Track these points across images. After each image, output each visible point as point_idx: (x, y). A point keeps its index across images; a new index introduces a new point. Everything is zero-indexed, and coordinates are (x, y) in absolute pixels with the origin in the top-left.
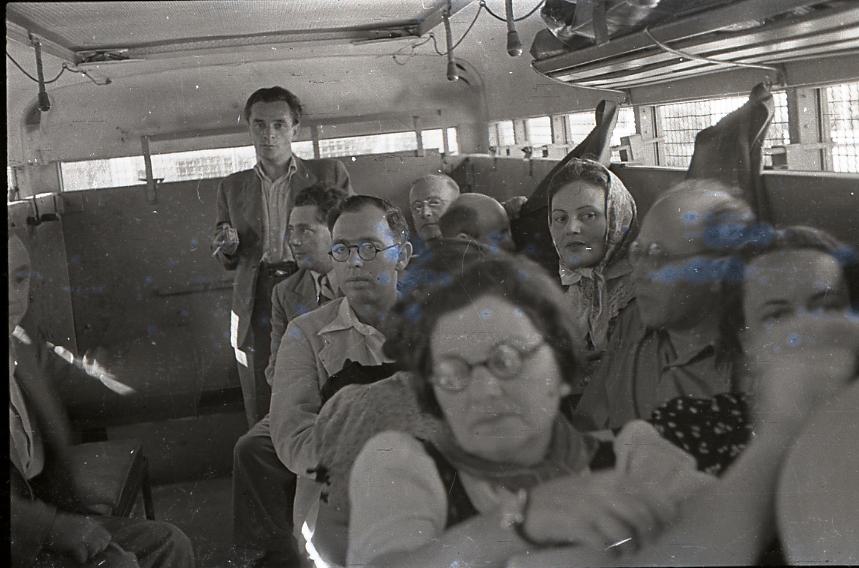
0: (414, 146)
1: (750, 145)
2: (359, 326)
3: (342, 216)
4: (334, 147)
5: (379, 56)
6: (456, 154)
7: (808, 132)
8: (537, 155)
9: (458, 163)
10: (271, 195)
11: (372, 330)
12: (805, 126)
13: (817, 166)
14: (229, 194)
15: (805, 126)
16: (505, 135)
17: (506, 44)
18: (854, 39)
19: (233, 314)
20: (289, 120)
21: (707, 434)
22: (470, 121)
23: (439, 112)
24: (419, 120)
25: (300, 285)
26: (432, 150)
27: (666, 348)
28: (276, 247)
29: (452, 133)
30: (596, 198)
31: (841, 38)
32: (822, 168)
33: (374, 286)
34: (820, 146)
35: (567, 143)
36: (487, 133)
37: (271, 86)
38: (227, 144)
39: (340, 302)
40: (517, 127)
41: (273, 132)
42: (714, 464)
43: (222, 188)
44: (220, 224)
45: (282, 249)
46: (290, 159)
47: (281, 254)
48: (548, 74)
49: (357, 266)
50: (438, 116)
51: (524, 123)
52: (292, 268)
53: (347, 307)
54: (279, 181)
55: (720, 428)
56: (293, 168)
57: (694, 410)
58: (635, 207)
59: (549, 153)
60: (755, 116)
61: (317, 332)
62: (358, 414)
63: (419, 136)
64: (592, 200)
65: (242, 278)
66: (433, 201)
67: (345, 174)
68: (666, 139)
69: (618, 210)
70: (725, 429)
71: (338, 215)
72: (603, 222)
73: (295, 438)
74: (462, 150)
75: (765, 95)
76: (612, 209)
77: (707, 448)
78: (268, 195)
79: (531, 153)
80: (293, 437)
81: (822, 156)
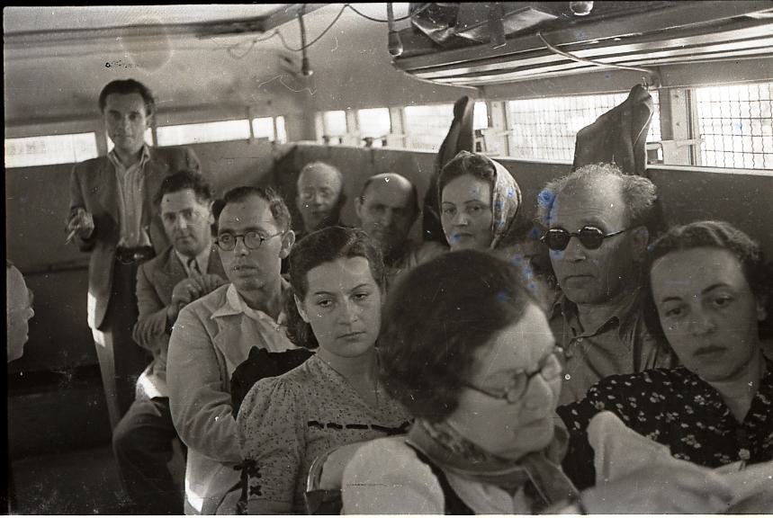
0: (247, 135)
2: (249, 311)
3: (226, 207)
4: (173, 135)
5: (215, 49)
7: (680, 130)
10: (126, 181)
11: (262, 315)
14: (83, 180)
15: (678, 124)
16: (334, 126)
17: (387, 43)
20: (142, 111)
21: (643, 403)
22: (298, 111)
24: (251, 110)
27: (574, 323)
28: (134, 233)
29: (281, 121)
31: (126, 29)
33: (260, 274)
34: (691, 142)
37: (126, 78)
38: (56, 132)
39: (226, 289)
41: (128, 123)
43: (76, 174)
44: (73, 208)
45: (139, 233)
46: (143, 148)
47: (138, 239)
48: (408, 72)
49: (243, 255)
50: (269, 109)
52: (149, 253)
53: (236, 295)
54: (133, 168)
55: (654, 397)
56: (146, 156)
57: (628, 384)
58: (520, 196)
59: (388, 142)
60: (633, 113)
61: (209, 317)
65: (99, 261)
67: (195, 162)
69: (504, 202)
71: (223, 206)
72: (489, 215)
73: (191, 420)
74: (290, 138)
75: (645, 96)
76: (497, 200)
77: (644, 416)
78: (122, 183)
80: (193, 422)
81: (691, 150)
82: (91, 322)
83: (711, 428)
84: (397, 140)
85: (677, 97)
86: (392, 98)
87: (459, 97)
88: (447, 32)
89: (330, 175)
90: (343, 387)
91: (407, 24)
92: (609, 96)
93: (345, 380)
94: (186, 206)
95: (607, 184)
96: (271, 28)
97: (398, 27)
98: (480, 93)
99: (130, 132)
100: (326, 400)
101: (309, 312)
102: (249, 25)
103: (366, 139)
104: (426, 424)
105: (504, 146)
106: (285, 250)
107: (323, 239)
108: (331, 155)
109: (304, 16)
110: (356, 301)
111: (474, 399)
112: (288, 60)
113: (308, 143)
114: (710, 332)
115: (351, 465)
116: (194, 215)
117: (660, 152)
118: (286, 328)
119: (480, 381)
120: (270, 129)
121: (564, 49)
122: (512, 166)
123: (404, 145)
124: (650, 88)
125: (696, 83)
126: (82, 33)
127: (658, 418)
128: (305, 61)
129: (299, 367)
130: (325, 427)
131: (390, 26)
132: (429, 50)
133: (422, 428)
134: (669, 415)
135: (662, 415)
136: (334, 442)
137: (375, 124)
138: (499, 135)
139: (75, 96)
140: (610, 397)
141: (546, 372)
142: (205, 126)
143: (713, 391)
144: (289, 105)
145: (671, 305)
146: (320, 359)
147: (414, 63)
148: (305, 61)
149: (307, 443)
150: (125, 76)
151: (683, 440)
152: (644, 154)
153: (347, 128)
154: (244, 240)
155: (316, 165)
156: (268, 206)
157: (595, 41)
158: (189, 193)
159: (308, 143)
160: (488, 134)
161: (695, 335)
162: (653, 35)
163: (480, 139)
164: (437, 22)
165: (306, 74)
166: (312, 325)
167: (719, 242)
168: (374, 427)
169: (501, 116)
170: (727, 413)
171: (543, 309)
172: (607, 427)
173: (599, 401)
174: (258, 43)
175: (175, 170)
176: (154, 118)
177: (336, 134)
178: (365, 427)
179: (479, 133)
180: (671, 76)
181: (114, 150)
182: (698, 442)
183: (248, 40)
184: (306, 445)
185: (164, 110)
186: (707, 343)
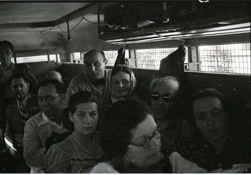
2: (50, 122)
4: (21, 60)
6: (60, 62)
7: (194, 59)
8: (77, 63)
13: (197, 70)
15: (194, 57)
18: (249, 31)
20: (10, 51)
24: (48, 52)
29: (58, 55)
30: (127, 76)
32: (198, 70)
34: (198, 63)
48: (103, 40)
50: (54, 51)
54: (9, 71)
56: (13, 67)
59: (80, 62)
60: (180, 54)
62: (60, 153)
64: (127, 77)
74: (62, 61)
75: (184, 48)
76: (132, 80)
85: (193, 49)
90: (81, 146)
91: (104, 24)
92: (170, 48)
94: (21, 83)
96: (57, 25)
97: (101, 25)
98: (127, 47)
99: (6, 58)
101: (75, 118)
105: (134, 64)
110: (91, 117)
113: (68, 63)
116: (23, 87)
117: (188, 67)
118: (7, 136)
119: (133, 140)
121: (157, 33)
122: (134, 70)
124: (185, 46)
128: (69, 36)
129: (66, 139)
131: (99, 25)
138: (133, 61)
141: (156, 136)
146: (73, 136)
148: (69, 36)
152: (184, 67)
153: (81, 58)
157: (167, 31)
159: (68, 63)
160: (129, 60)
162: (185, 30)
168: (92, 160)
169: (196, 53)
172: (175, 155)
177: (77, 60)
179: (126, 59)
180: (190, 42)
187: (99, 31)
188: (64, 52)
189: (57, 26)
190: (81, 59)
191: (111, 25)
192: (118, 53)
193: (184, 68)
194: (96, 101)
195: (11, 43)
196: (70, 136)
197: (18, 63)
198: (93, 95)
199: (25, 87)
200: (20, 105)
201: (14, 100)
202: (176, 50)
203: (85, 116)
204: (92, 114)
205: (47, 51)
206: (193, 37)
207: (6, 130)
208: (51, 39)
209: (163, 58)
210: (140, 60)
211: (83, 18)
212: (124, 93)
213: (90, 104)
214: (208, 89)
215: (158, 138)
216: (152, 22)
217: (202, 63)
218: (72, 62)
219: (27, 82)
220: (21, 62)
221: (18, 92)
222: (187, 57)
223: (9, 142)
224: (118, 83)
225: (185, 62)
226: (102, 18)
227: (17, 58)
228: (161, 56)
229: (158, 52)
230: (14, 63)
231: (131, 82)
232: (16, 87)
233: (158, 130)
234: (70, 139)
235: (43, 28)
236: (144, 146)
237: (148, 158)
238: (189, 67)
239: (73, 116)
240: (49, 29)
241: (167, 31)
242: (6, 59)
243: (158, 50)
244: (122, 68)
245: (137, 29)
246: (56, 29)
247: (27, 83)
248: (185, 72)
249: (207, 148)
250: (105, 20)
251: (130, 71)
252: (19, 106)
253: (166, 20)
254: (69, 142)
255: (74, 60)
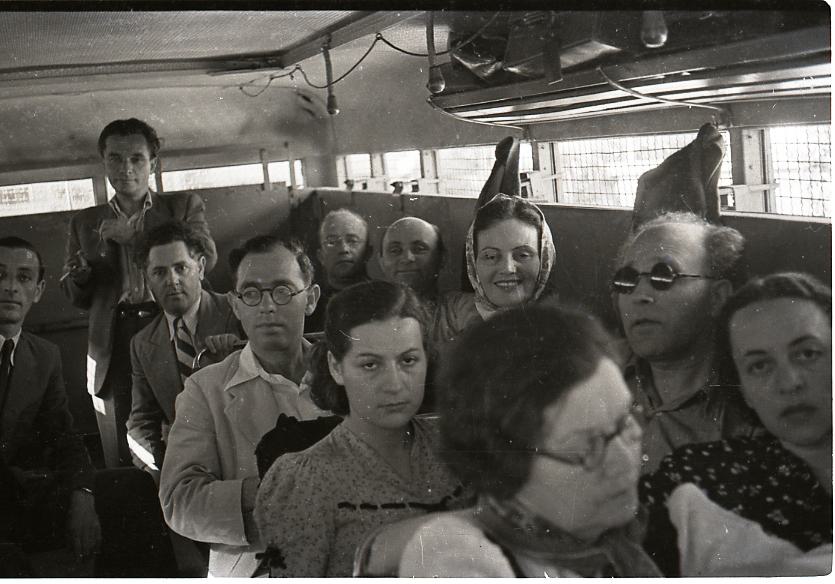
1: (704, 185)
2: (265, 375)
4: (176, 181)
6: (301, 188)
7: (752, 174)
8: (358, 188)
9: (305, 197)
11: (279, 378)
12: (750, 167)
13: (762, 210)
15: (750, 167)
16: (356, 169)
19: (89, 359)
20: (146, 155)
21: (724, 476)
23: (286, 145)
24: (265, 154)
25: (156, 333)
26: (278, 183)
29: (298, 164)
32: (766, 210)
34: (765, 187)
35: (437, 178)
36: (335, 167)
37: (129, 118)
40: (374, 160)
41: (131, 167)
42: (736, 506)
46: (146, 195)
48: (446, 110)
50: (284, 149)
51: (382, 156)
54: (134, 217)
55: (736, 468)
56: (148, 203)
57: (705, 453)
60: (703, 155)
63: (265, 169)
65: (97, 318)
66: (350, 238)
68: (564, 176)
70: (742, 470)
74: (308, 184)
76: (546, 248)
79: (402, 188)
82: (91, 389)
83: (800, 502)
84: (429, 184)
85: (750, 137)
86: (428, 138)
87: (501, 138)
88: (493, 66)
89: (355, 223)
90: (374, 461)
91: (447, 58)
93: (376, 452)
94: (179, 260)
95: (688, 231)
99: (132, 177)
100: (357, 476)
101: (345, 372)
102: (266, 60)
103: (394, 184)
104: (492, 501)
106: (310, 306)
107: (353, 294)
108: (357, 201)
109: (330, 51)
110: (404, 368)
111: (546, 468)
112: (307, 99)
114: (799, 388)
115: (410, 549)
116: (186, 270)
119: (552, 445)
120: (287, 173)
121: (627, 85)
123: (438, 192)
124: (721, 127)
125: (773, 122)
126: (81, 69)
127: (741, 491)
128: (331, 98)
129: (324, 439)
130: (358, 509)
131: (431, 61)
132: (472, 86)
133: (487, 504)
134: (752, 488)
135: (745, 488)
136: (370, 525)
137: (402, 166)
139: (72, 138)
140: (687, 468)
141: (626, 434)
142: (205, 171)
143: (798, 460)
144: (309, 150)
145: (751, 359)
147: (455, 100)
148: (331, 98)
149: (338, 527)
150: (125, 114)
151: (769, 516)
152: (717, 198)
153: (372, 173)
154: (271, 295)
155: (339, 213)
156: (295, 258)
158: (181, 246)
160: (534, 177)
161: (782, 392)
162: (722, 71)
163: (527, 184)
164: (482, 57)
165: (331, 112)
166: (350, 393)
167: (805, 290)
168: (412, 505)
170: (816, 486)
171: (616, 363)
172: (689, 500)
173: (675, 472)
174: (274, 81)
175: (172, 217)
176: (158, 162)
178: (402, 506)
179: (524, 176)
181: (115, 197)
182: (786, 517)
183: (265, 76)
184: (336, 529)
185: (174, 153)
186: (796, 401)
187: (432, 80)
188: (317, 154)
189: (293, 67)
190: (372, 176)
191: (472, 61)
192: (498, 153)
193: (716, 203)
194: (414, 313)
195: (152, 130)
196: (337, 430)
197: (170, 190)
198: (403, 291)
199: (190, 269)
200: (176, 329)
201: (155, 310)
202: (690, 142)
203: (382, 369)
204: (405, 359)
205: (262, 150)
206: (745, 96)
207: (133, 409)
208: (271, 110)
209: (647, 169)
210: (569, 177)
211: (378, 39)
212: (520, 294)
213: (393, 323)
214: (781, 275)
215: (633, 439)
216: (608, 48)
217: (781, 185)
218: (342, 187)
219: (197, 252)
220: (176, 190)
221: (170, 292)
222: (726, 167)
223: (141, 447)
224: (499, 257)
225: (719, 181)
226: (442, 35)
227: (164, 175)
228: (639, 162)
229: (630, 149)
230: (155, 191)
231: (542, 253)
232: (162, 271)
233: (632, 412)
234: (338, 439)
235: (247, 74)
236: (588, 461)
237: (598, 504)
238: (734, 198)
239: (342, 367)
240: (265, 76)
241: (660, 76)
242: (130, 178)
243: (631, 143)
244: (512, 206)
245: (556, 70)
246: (289, 79)
247: (196, 257)
248: (723, 216)
249: (787, 474)
250: (452, 44)
251: (539, 217)
252: (172, 335)
253: (656, 40)
254: (334, 451)
255: (350, 178)
